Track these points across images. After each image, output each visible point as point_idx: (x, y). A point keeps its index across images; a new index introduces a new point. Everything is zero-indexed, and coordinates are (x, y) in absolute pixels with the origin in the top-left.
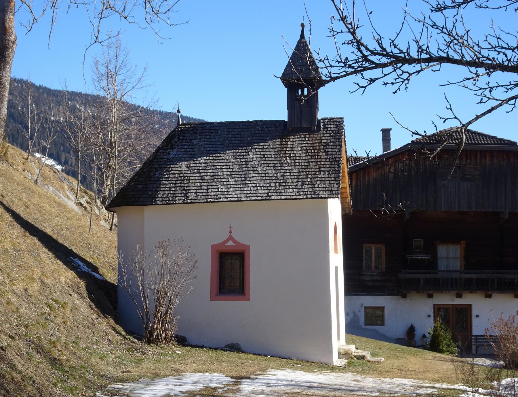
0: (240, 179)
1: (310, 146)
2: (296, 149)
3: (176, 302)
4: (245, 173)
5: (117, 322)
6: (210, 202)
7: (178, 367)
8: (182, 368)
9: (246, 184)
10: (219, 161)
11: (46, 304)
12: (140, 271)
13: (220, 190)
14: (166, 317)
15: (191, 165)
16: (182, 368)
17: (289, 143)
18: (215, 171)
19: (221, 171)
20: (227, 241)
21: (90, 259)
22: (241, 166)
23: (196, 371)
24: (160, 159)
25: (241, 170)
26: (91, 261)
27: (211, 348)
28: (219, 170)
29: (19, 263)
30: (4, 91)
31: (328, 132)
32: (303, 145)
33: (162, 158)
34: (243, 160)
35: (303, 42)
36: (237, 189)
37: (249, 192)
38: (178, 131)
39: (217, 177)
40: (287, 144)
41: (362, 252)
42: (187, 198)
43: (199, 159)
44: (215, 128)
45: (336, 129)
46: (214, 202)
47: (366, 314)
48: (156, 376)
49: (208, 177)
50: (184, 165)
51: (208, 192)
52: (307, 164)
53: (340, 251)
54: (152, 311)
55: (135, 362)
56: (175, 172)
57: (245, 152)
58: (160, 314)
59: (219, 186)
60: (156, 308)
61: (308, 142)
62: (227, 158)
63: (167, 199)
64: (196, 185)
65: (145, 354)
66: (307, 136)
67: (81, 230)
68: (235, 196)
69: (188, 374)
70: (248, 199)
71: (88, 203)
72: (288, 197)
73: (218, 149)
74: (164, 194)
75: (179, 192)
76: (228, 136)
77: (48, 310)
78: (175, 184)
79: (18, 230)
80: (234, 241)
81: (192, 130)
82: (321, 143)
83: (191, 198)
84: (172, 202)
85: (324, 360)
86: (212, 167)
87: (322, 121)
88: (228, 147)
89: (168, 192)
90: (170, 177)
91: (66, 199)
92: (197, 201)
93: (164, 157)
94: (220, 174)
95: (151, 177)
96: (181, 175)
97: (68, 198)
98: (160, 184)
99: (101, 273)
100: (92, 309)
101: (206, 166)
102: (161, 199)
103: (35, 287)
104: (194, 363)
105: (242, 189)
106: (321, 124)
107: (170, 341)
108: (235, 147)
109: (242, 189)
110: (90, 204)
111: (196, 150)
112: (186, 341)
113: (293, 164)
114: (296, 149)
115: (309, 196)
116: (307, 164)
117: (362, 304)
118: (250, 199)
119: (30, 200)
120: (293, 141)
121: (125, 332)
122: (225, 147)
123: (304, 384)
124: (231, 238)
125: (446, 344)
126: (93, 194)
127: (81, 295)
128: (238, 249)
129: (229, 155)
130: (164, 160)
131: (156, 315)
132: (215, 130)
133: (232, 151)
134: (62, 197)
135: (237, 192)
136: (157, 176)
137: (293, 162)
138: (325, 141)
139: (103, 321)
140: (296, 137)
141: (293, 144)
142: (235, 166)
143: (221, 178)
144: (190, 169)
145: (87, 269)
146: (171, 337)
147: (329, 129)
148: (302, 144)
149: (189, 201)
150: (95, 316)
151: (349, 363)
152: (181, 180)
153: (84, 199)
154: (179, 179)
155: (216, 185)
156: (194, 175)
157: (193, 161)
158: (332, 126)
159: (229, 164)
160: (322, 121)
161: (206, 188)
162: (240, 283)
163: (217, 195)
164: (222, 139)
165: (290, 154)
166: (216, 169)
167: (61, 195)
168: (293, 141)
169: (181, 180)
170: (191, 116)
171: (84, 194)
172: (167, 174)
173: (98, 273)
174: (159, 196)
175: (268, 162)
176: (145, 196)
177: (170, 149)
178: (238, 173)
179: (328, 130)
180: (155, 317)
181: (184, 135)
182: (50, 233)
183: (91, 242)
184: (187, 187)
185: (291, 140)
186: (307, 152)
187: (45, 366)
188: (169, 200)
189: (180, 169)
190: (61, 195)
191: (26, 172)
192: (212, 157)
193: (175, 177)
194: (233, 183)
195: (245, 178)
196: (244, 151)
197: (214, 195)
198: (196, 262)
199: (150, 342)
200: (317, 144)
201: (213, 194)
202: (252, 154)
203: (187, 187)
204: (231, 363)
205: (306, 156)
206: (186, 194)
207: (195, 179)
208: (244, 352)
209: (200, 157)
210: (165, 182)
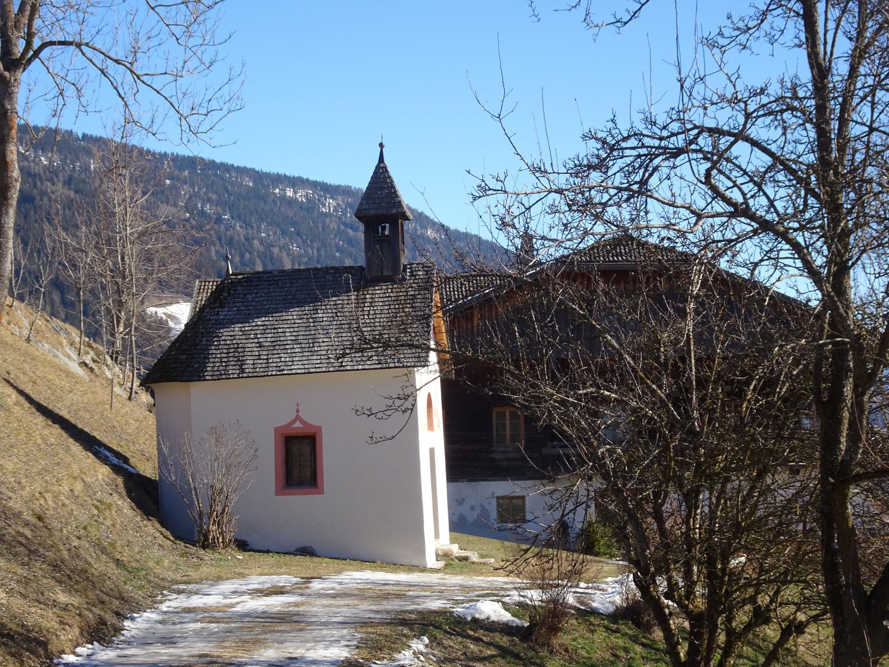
0: (307, 346)
1: (394, 300)
2: (376, 304)
3: (234, 498)
4: (313, 336)
5: (163, 526)
6: (272, 375)
7: (241, 571)
8: (247, 572)
9: (315, 351)
10: (280, 322)
11: (93, 505)
12: (189, 463)
13: (283, 359)
14: (222, 517)
15: (247, 328)
16: (247, 572)
17: (368, 296)
18: (276, 335)
19: (283, 335)
20: (293, 422)
21: (117, 447)
22: (308, 329)
23: (261, 574)
24: (207, 320)
25: (308, 333)
26: (119, 449)
27: (277, 553)
28: (281, 334)
29: (57, 460)
30: (7, 242)
31: (416, 281)
32: (385, 299)
33: (210, 320)
34: (311, 320)
35: (382, 168)
36: (304, 358)
37: (319, 362)
38: (228, 283)
39: (279, 343)
40: (366, 298)
41: (492, 419)
42: (243, 371)
43: (256, 320)
44: (274, 278)
45: (426, 277)
46: (276, 375)
47: (499, 505)
48: (219, 579)
49: (267, 344)
50: (237, 329)
51: (268, 363)
52: (389, 324)
53: (439, 426)
54: (206, 510)
55: (192, 568)
56: (227, 338)
57: (313, 310)
58: (215, 513)
59: (282, 355)
60: (211, 507)
61: (391, 295)
62: (291, 317)
63: (218, 373)
64: (254, 353)
65: (201, 559)
66: (390, 287)
67: (100, 409)
68: (302, 367)
69: (253, 577)
70: (318, 370)
71: (94, 361)
72: (366, 367)
73: (279, 306)
74: (215, 366)
75: (233, 363)
76: (291, 289)
77: (96, 512)
78: (227, 353)
79: (40, 419)
80: (302, 421)
81: (245, 282)
82: (407, 295)
83: (247, 371)
84: (224, 377)
85: (415, 563)
86: (273, 331)
87: (408, 267)
88: (292, 303)
89: (219, 364)
90: (220, 344)
91: (66, 360)
92: (255, 374)
93: (212, 318)
94: (282, 339)
95: (197, 345)
96: (234, 342)
97: (69, 357)
98: (209, 354)
99: (133, 465)
100: (134, 510)
101: (265, 330)
102: (210, 373)
103: (79, 487)
104: (259, 567)
105: (310, 358)
106: (408, 270)
107: (229, 545)
108: (300, 303)
109: (310, 358)
110: (98, 362)
111: (251, 308)
112: (248, 545)
113: (372, 325)
114: (376, 304)
115: (392, 365)
116: (389, 324)
117: (493, 493)
118: (320, 370)
119: (34, 372)
120: (373, 294)
121: (173, 536)
122: (288, 304)
123: (380, 582)
124: (298, 418)
125: (605, 544)
126: (101, 348)
127: (120, 494)
128: (308, 431)
129: (293, 313)
130: (211, 322)
131: (211, 514)
132: (275, 281)
133: (297, 309)
134: (62, 357)
135: (304, 362)
136: (204, 343)
137: (372, 321)
138: (412, 293)
139: (149, 523)
140: (377, 288)
141: (372, 298)
142: (301, 329)
143: (284, 345)
144: (245, 333)
145: (117, 460)
146: (230, 540)
147: (417, 277)
148: (383, 297)
149: (245, 375)
150: (138, 519)
151: (446, 565)
152: (234, 348)
153: (89, 357)
154: (232, 346)
155: (278, 354)
156: (251, 341)
157: (249, 323)
158: (421, 273)
159: (293, 326)
160: (408, 267)
161: (265, 357)
162: (311, 473)
163: (280, 367)
164: (283, 294)
165: (369, 311)
166: (278, 332)
167: (59, 354)
168: (373, 294)
169: (234, 348)
170: (230, 163)
171: (87, 349)
172: (217, 341)
173: (129, 465)
174: (208, 369)
175: (342, 322)
176: (190, 369)
177: (218, 307)
178: (305, 337)
179: (416, 279)
180: (209, 518)
181: (236, 288)
182: (67, 417)
183: (116, 424)
184: (242, 356)
185: (370, 292)
186: (390, 308)
187: (112, 565)
188: (221, 374)
189: (232, 334)
190: (59, 354)
191: (12, 325)
192: (272, 317)
193: (227, 344)
194: (299, 350)
195: (313, 343)
196: (312, 308)
197: (276, 367)
198: (256, 451)
199: (204, 547)
200: (403, 298)
201: (275, 365)
202: (322, 312)
203: (242, 356)
204: (302, 566)
205: (388, 313)
206: (241, 365)
207: (251, 346)
208: (318, 556)
209: (257, 318)
210: (214, 352)
